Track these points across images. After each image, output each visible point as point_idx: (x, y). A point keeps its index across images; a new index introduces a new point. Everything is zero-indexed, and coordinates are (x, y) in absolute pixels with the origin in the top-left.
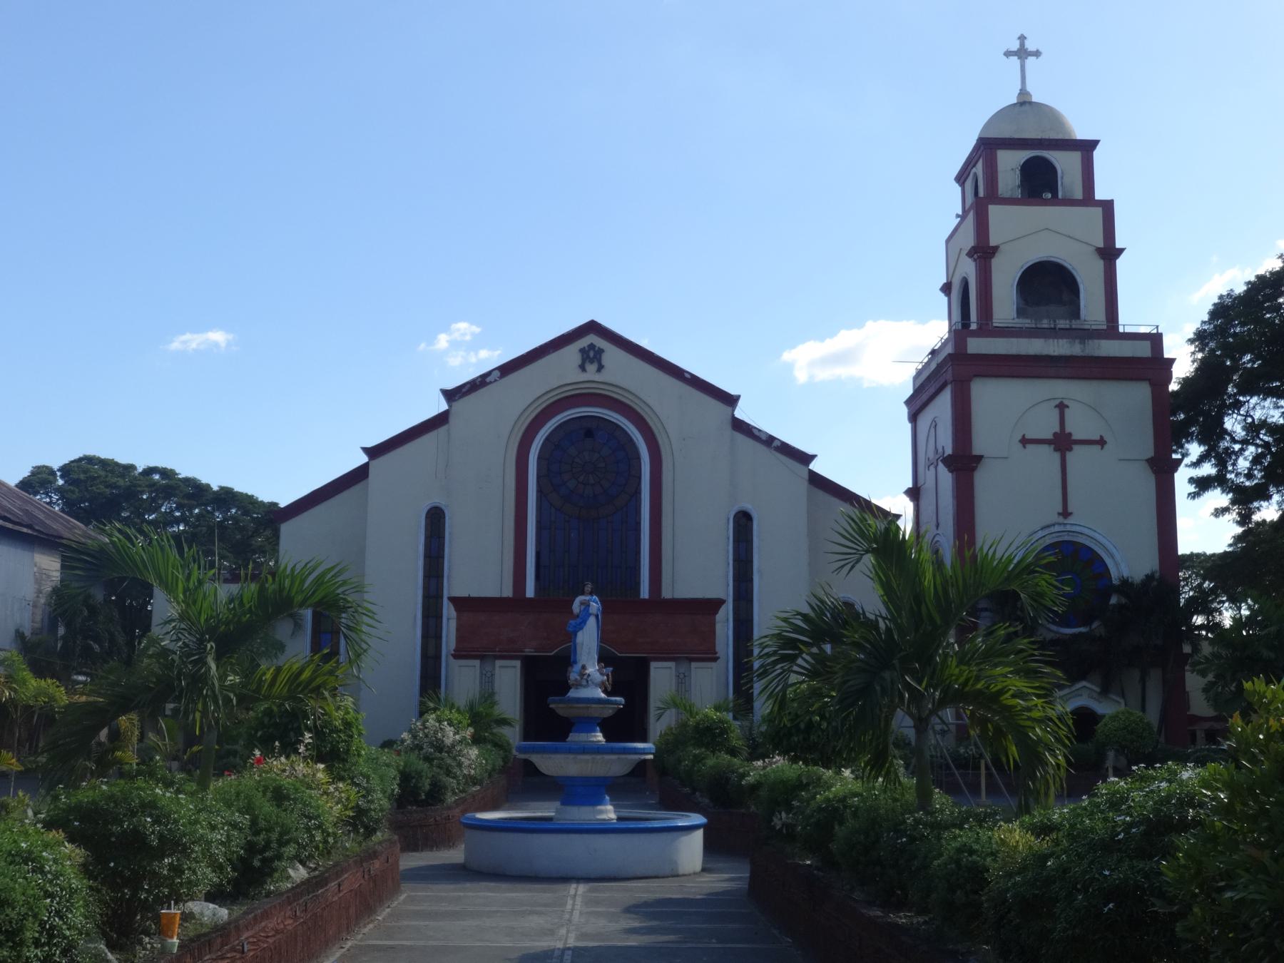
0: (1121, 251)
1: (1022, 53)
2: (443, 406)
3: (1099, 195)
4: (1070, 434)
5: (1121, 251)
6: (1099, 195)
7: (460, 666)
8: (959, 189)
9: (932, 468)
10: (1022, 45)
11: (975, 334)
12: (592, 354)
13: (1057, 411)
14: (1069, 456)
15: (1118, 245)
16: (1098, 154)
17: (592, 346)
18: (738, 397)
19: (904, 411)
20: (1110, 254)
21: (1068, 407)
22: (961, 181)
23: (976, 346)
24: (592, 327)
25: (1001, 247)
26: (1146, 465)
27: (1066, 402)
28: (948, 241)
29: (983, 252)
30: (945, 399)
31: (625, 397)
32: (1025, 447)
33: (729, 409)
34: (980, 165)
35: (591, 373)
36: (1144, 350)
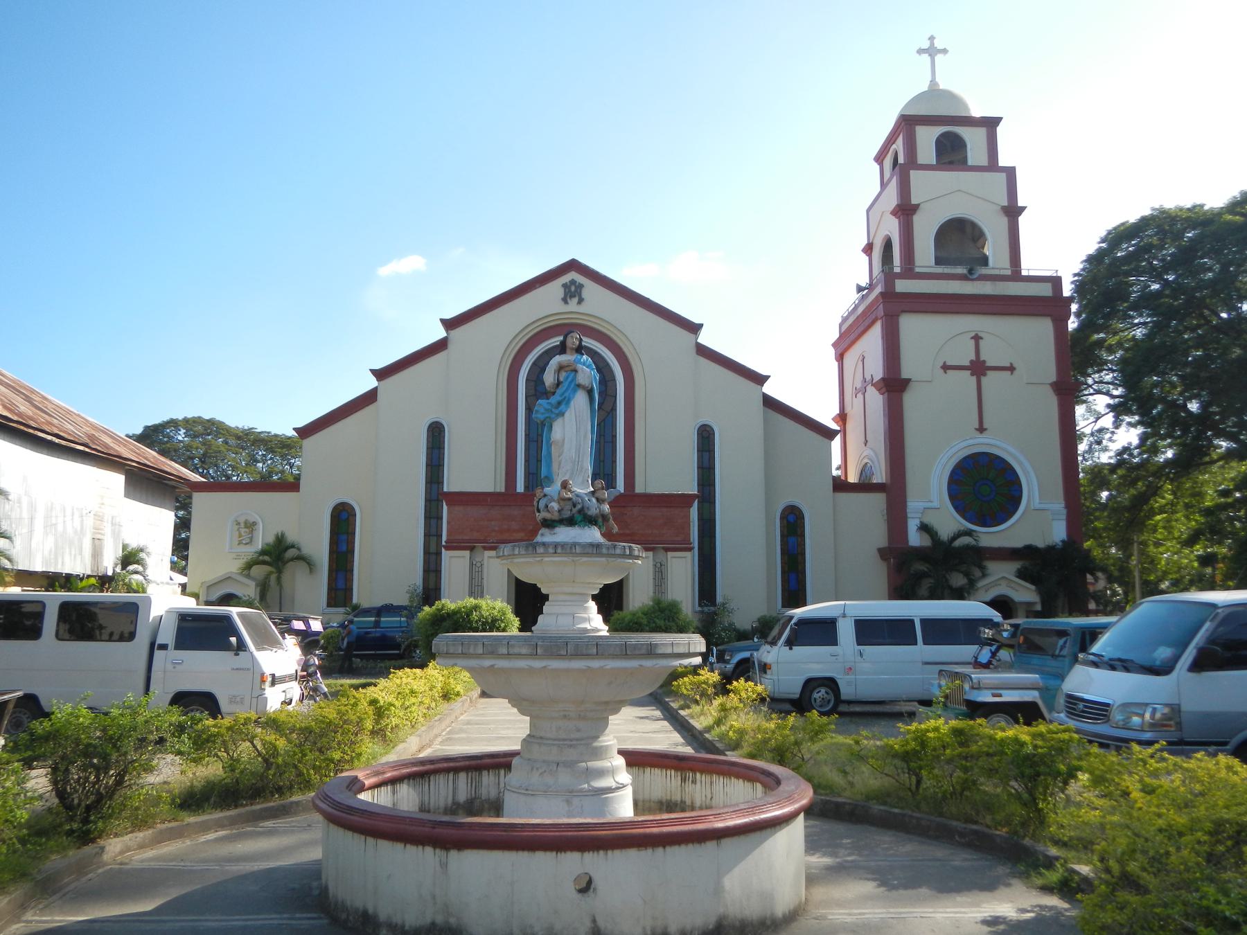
0: (1023, 208)
1: (932, 51)
2: (441, 333)
3: (1003, 162)
4: (984, 362)
5: (1023, 208)
6: (1003, 162)
7: (451, 557)
8: (877, 167)
9: (860, 396)
10: (932, 44)
11: (901, 276)
12: (573, 289)
13: (973, 342)
14: (984, 380)
15: (1020, 204)
16: (1001, 130)
17: (573, 282)
18: (701, 325)
19: (832, 352)
20: (1013, 212)
21: (982, 338)
22: (880, 161)
23: (902, 286)
24: (572, 265)
25: (921, 206)
26: (1048, 387)
27: (980, 334)
28: (868, 211)
29: (906, 211)
30: (875, 334)
31: (601, 325)
32: (946, 373)
33: (692, 336)
34: (900, 141)
35: (573, 305)
36: (1045, 290)
